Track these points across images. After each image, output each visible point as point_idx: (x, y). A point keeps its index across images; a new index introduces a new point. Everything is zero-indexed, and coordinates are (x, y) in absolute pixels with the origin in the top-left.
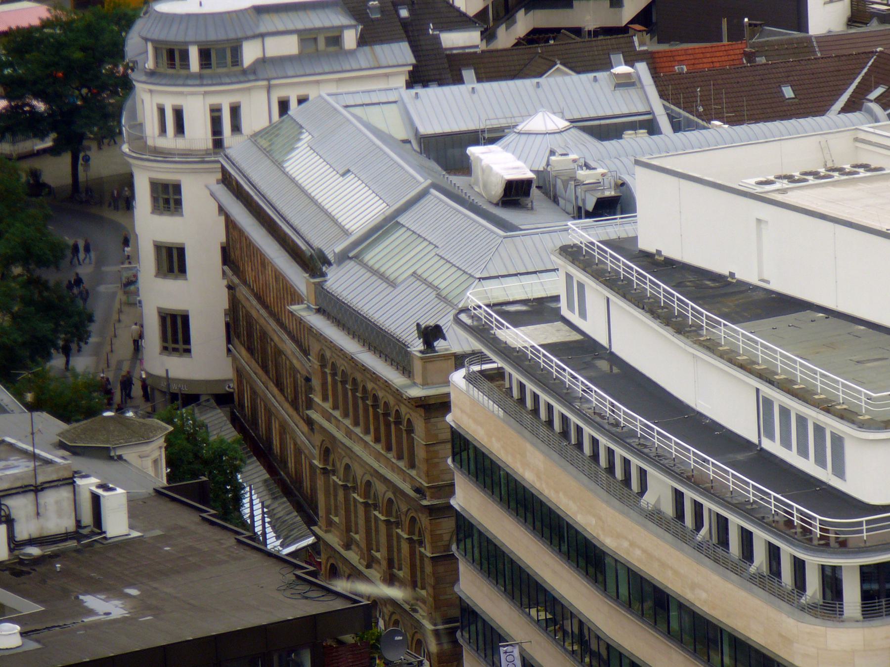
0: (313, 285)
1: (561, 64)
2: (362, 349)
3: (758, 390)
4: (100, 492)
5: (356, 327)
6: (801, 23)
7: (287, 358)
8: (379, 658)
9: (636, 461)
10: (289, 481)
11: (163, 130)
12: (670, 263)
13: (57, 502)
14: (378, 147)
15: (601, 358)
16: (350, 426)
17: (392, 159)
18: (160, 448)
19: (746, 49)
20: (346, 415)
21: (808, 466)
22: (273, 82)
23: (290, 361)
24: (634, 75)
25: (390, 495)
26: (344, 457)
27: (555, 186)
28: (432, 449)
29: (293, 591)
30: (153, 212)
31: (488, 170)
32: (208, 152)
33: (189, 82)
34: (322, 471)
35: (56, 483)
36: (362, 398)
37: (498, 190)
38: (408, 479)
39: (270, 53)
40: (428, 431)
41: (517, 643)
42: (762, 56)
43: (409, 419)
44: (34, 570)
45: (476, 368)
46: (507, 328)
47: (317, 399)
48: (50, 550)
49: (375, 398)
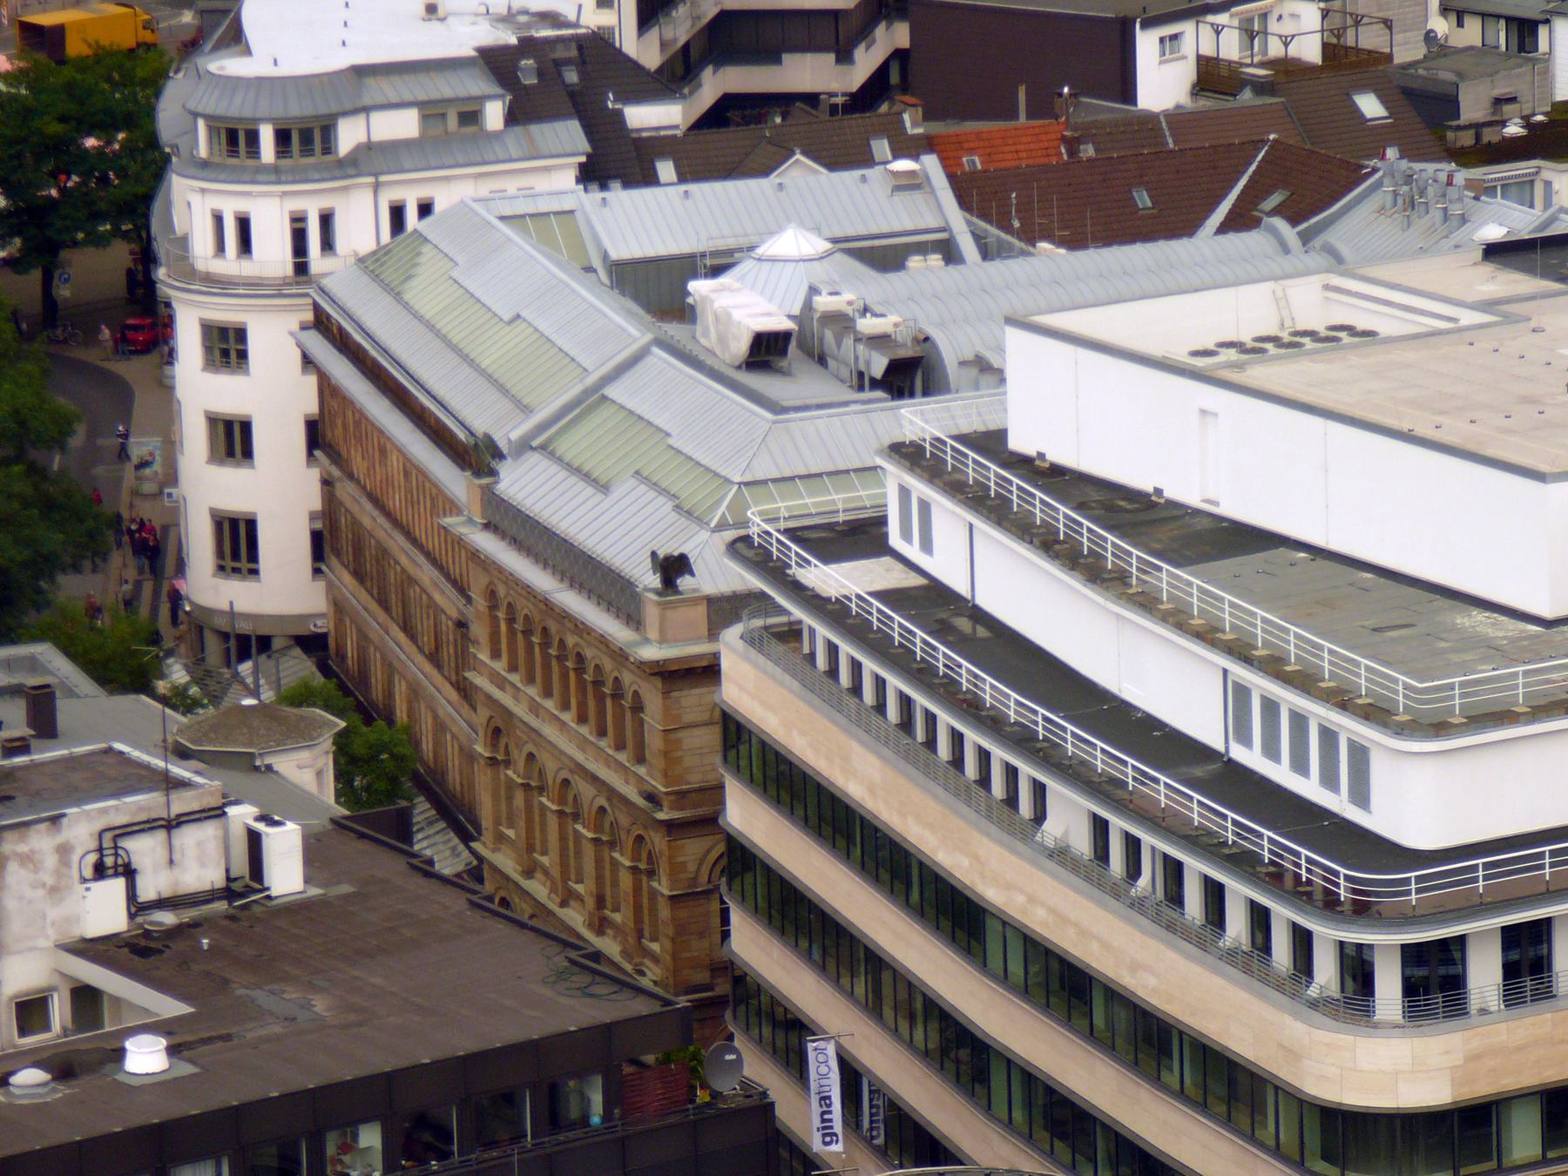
0: (479, 490)
1: (804, 153)
2: (561, 586)
3: (1225, 672)
4: (260, 827)
5: (541, 546)
6: (1126, 88)
7: (423, 590)
8: (701, 1088)
9: (1028, 769)
10: (422, 771)
11: (220, 247)
12: (1057, 471)
13: (199, 844)
14: (562, 281)
15: (961, 615)
16: (537, 699)
17: (585, 300)
18: (327, 753)
19: (1066, 133)
20: (530, 680)
21: (1309, 788)
22: (383, 178)
23: (428, 594)
24: (921, 174)
25: (602, 801)
26: (526, 742)
27: (821, 340)
28: (672, 736)
29: (568, 984)
30: (205, 369)
31: (723, 319)
32: (288, 281)
33: (260, 177)
34: (488, 761)
35: (197, 816)
36: (558, 657)
37: (741, 346)
38: (632, 780)
39: (378, 136)
40: (666, 710)
41: (833, 1037)
42: (1087, 143)
43: (636, 692)
44: (168, 947)
45: (758, 623)
46: (816, 566)
47: (484, 656)
48: (188, 915)
49: (580, 658)
